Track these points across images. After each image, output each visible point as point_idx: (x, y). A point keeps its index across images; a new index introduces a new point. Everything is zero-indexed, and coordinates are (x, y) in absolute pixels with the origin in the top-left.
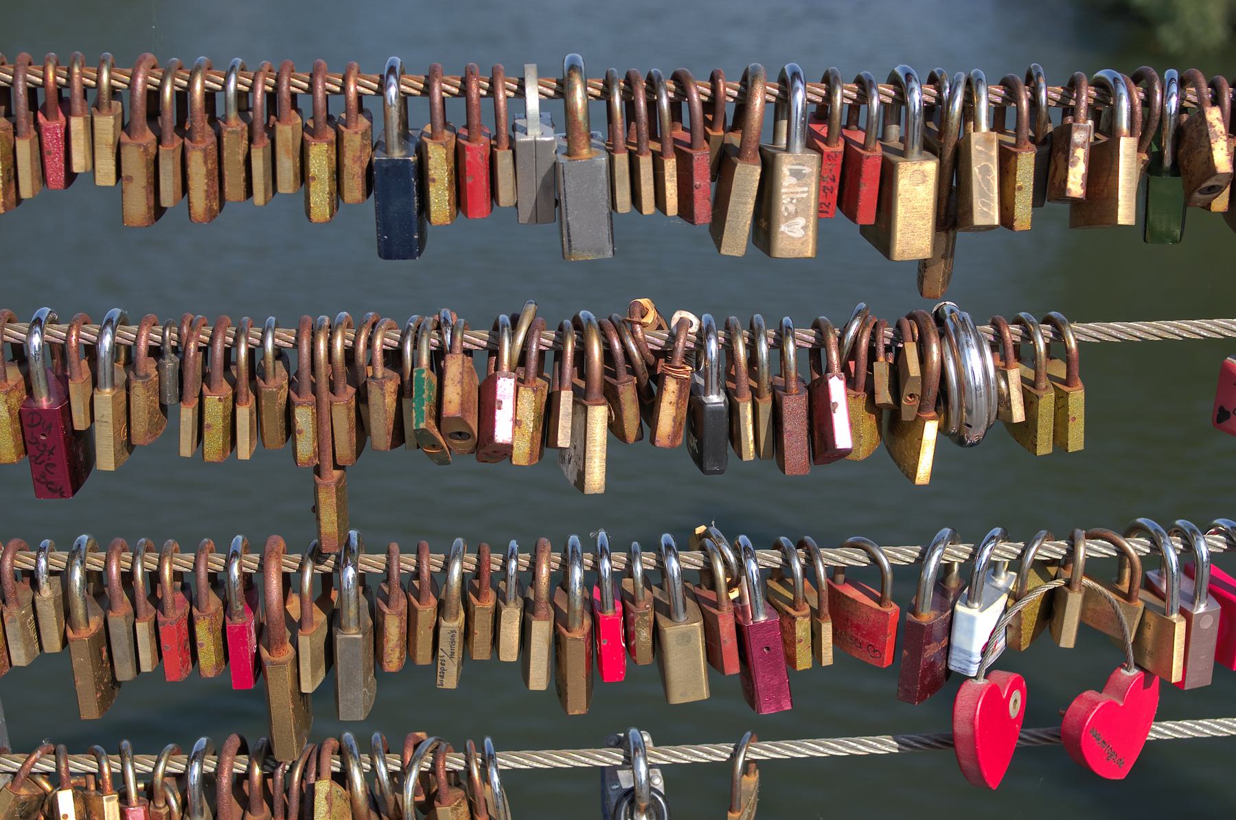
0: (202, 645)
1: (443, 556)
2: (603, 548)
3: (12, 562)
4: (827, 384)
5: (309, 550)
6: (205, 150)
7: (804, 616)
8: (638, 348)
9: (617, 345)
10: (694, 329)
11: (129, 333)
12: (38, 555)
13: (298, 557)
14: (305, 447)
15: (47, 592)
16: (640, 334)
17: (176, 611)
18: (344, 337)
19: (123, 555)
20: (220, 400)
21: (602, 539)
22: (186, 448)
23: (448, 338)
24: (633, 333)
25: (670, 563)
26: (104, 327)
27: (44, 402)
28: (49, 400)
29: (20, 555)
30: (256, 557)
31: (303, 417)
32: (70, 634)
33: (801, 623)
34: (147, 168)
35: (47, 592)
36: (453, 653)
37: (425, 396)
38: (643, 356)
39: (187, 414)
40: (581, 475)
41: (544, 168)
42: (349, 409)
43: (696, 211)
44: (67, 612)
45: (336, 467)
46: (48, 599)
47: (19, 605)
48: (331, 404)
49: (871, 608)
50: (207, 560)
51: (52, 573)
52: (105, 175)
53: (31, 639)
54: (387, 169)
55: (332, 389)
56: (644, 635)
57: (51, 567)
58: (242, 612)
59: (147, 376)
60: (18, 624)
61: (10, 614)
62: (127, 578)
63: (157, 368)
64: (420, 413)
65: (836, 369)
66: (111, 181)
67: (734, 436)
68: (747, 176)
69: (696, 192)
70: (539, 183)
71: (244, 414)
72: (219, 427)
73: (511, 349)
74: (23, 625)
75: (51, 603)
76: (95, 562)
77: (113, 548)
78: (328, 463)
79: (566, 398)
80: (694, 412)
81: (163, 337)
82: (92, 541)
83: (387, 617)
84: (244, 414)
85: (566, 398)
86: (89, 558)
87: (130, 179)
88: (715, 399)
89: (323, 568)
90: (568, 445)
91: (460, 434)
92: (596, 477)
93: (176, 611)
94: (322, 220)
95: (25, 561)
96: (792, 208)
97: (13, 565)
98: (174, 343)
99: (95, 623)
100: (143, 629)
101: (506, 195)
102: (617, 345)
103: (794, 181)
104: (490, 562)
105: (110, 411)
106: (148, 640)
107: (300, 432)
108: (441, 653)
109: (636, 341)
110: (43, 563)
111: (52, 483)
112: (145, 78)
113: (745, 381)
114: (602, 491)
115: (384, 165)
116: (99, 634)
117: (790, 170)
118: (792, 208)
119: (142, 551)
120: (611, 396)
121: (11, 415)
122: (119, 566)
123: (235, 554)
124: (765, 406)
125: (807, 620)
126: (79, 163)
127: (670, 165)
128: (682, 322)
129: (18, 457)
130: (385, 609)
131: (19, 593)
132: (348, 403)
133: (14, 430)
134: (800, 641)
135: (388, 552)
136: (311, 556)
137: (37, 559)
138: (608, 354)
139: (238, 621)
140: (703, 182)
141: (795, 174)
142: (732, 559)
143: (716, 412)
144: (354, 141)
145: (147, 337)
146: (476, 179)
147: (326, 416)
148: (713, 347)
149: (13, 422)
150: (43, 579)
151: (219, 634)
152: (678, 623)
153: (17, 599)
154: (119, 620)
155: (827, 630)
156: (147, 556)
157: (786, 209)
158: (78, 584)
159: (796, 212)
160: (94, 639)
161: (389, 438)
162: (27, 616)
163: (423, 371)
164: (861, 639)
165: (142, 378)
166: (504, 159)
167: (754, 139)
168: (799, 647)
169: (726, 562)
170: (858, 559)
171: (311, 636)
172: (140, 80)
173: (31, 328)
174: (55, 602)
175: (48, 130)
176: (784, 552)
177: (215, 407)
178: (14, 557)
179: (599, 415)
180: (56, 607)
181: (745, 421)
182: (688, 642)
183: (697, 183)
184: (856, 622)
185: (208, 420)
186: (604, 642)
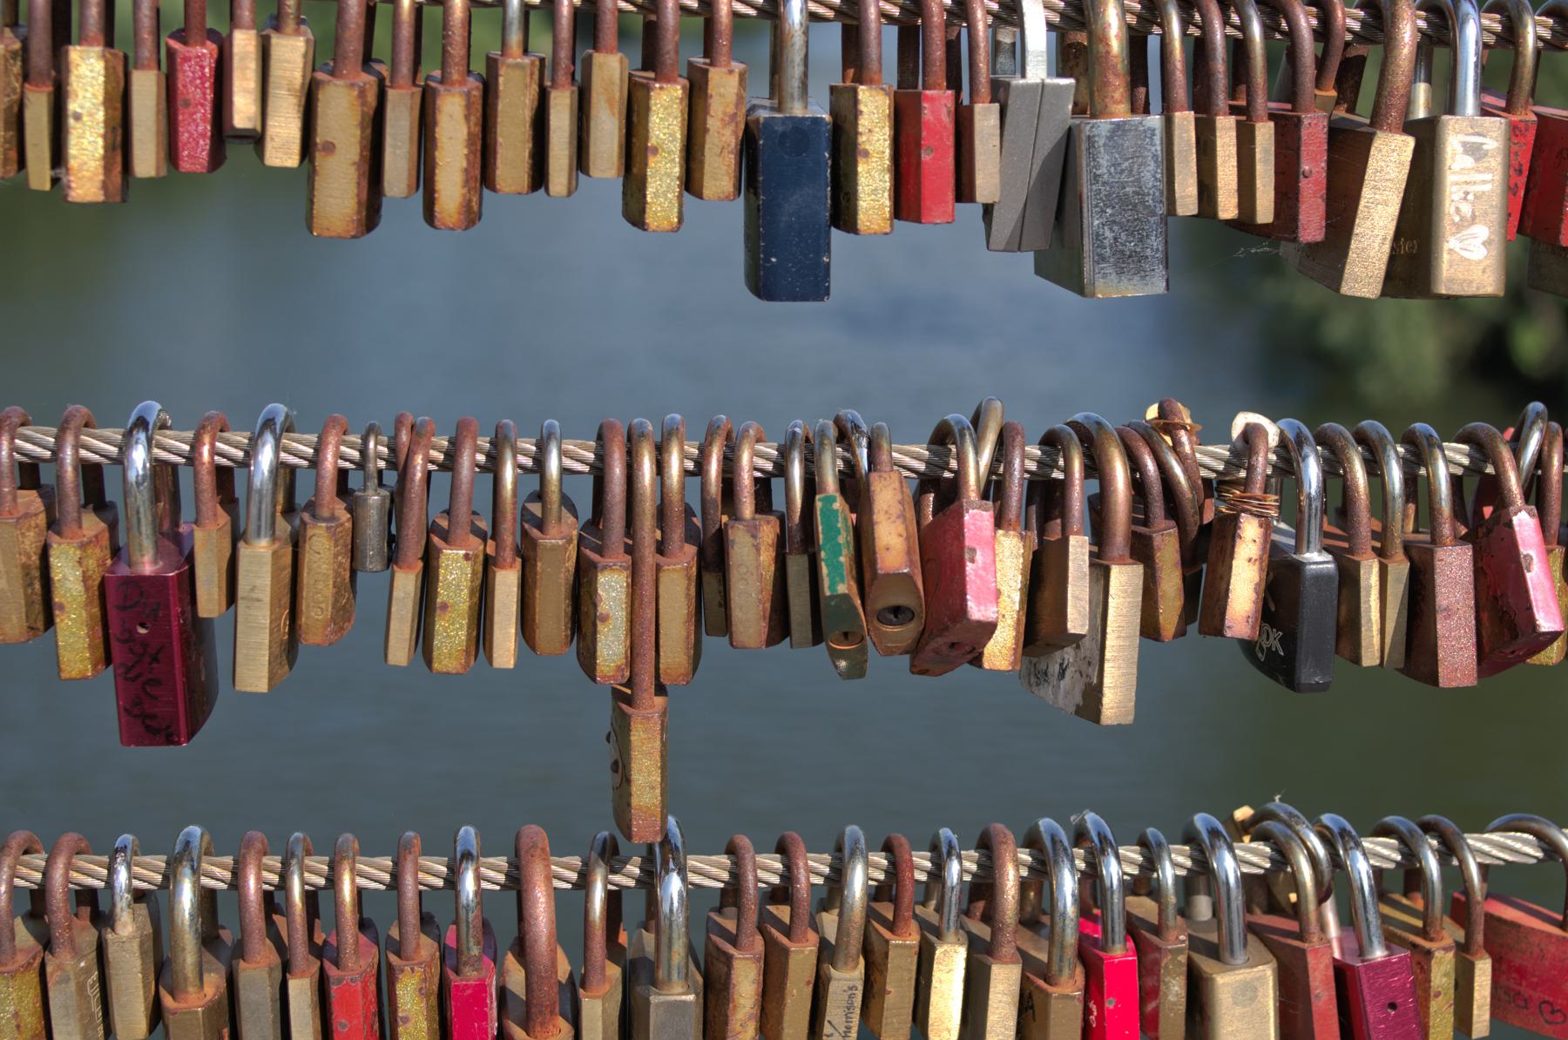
0: (406, 1020)
1: (827, 857)
2: (1103, 838)
3: (67, 873)
4: (1510, 524)
5: (598, 845)
6: (468, 94)
7: (1446, 949)
8: (1185, 471)
9: (1150, 466)
10: (1273, 440)
11: (301, 446)
12: (113, 860)
13: (576, 861)
14: (611, 647)
15: (128, 926)
16: (1187, 449)
17: (358, 962)
18: (684, 456)
19: (266, 860)
20: (467, 557)
21: (1095, 823)
22: (400, 651)
23: (863, 454)
24: (1176, 447)
25: (1221, 861)
26: (261, 434)
27: (147, 565)
28: (155, 562)
29: (80, 862)
30: (502, 862)
31: (611, 588)
32: (168, 1001)
33: (1440, 963)
34: (362, 126)
35: (128, 926)
36: (849, 1028)
37: (841, 539)
38: (1193, 486)
39: (406, 583)
40: (1094, 694)
41: (1050, 138)
42: (689, 579)
43: (1302, 218)
44: (161, 968)
45: (660, 690)
46: (130, 939)
47: (76, 953)
48: (658, 568)
49: (1550, 936)
50: (419, 868)
51: (139, 896)
52: (283, 149)
53: (92, 1015)
54: (784, 135)
55: (661, 548)
56: (1175, 990)
57: (136, 883)
58: (478, 959)
59: (333, 518)
60: (72, 986)
61: (60, 967)
62: (273, 902)
63: (350, 510)
64: (835, 567)
65: (1519, 501)
66: (292, 161)
67: (1349, 628)
68: (1390, 157)
69: (1303, 183)
70: (1036, 168)
71: (507, 583)
72: (465, 613)
73: (977, 463)
74: (81, 988)
75: (135, 946)
76: (217, 874)
77: (249, 845)
78: (646, 680)
79: (1079, 548)
80: (1281, 577)
81: (363, 452)
82: (206, 838)
83: (737, 964)
84: (507, 583)
85: (1079, 548)
86: (205, 866)
87: (330, 148)
88: (1316, 559)
89: (617, 878)
90: (1084, 630)
91: (896, 610)
92: (1117, 699)
93: (358, 962)
94: (665, 225)
95: (90, 873)
96: (1466, 209)
97: (68, 880)
98: (382, 464)
99: (213, 984)
100: (301, 991)
101: (987, 183)
102: (1150, 466)
103: (1469, 161)
104: (913, 867)
105: (268, 581)
106: (308, 1012)
107: (605, 619)
108: (827, 1029)
109: (1182, 458)
110: (122, 877)
111: (153, 717)
112: (213, 446)
113: (1365, 522)
114: (1129, 719)
115: (780, 128)
116: (219, 1002)
117: (1464, 144)
118: (1466, 209)
119: (299, 851)
120: (1141, 550)
121: (87, 589)
122: (259, 879)
123: (467, 856)
124: (1400, 569)
125: (1451, 955)
126: (243, 111)
127: (1265, 134)
128: (1250, 434)
129: (95, 667)
130: (731, 950)
131: (75, 932)
132: (688, 568)
133: (91, 617)
134: (1438, 995)
135: (731, 850)
136: (602, 855)
137: (111, 870)
138: (1138, 486)
139: (471, 975)
140: (1313, 163)
141: (1474, 151)
142: (1321, 851)
143: (1320, 578)
144: (724, 86)
145: (339, 453)
146: (936, 158)
147: (648, 591)
148: (1312, 471)
149: (88, 603)
150: (123, 900)
151: (434, 1001)
152: (1234, 968)
153: (72, 940)
154: (257, 976)
155: (1483, 970)
156: (308, 861)
157: (1458, 210)
158: (187, 916)
159: (1474, 217)
160: (211, 1010)
161: (763, 626)
162: (87, 971)
163: (831, 499)
164: (1525, 990)
165: (325, 520)
166: (986, 118)
167: (1402, 91)
168: (1434, 1005)
169: (1313, 859)
170: (1525, 847)
171: (604, 999)
172: (206, 450)
173: (128, 435)
174: (142, 945)
175: (186, 59)
176: (1402, 840)
177: (456, 569)
178: (69, 866)
179: (1124, 580)
180: (143, 953)
181: (1369, 595)
182: (1253, 999)
183: (1305, 167)
184: (1517, 961)
185: (443, 594)
186: (1110, 1004)
